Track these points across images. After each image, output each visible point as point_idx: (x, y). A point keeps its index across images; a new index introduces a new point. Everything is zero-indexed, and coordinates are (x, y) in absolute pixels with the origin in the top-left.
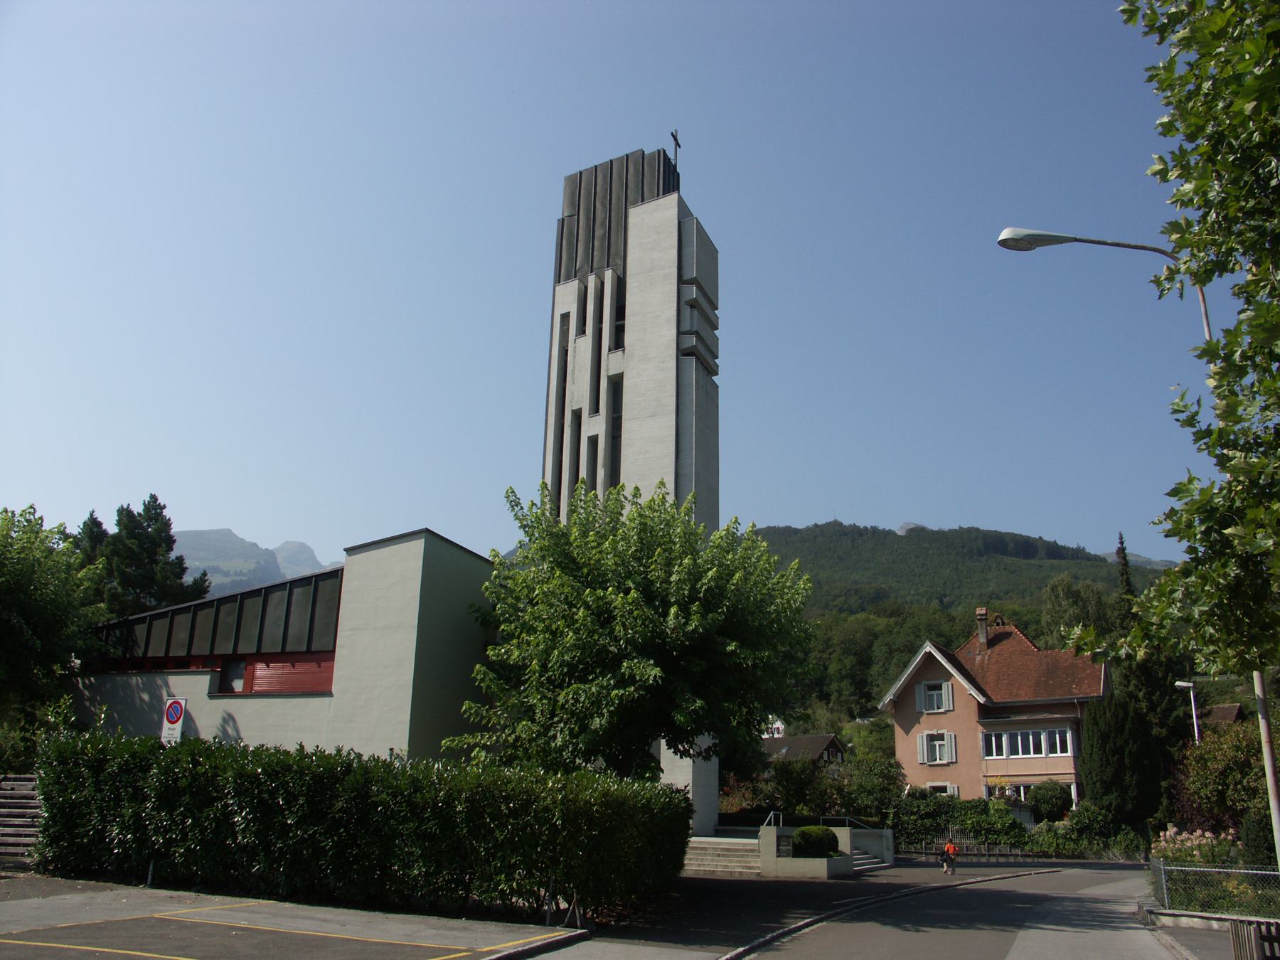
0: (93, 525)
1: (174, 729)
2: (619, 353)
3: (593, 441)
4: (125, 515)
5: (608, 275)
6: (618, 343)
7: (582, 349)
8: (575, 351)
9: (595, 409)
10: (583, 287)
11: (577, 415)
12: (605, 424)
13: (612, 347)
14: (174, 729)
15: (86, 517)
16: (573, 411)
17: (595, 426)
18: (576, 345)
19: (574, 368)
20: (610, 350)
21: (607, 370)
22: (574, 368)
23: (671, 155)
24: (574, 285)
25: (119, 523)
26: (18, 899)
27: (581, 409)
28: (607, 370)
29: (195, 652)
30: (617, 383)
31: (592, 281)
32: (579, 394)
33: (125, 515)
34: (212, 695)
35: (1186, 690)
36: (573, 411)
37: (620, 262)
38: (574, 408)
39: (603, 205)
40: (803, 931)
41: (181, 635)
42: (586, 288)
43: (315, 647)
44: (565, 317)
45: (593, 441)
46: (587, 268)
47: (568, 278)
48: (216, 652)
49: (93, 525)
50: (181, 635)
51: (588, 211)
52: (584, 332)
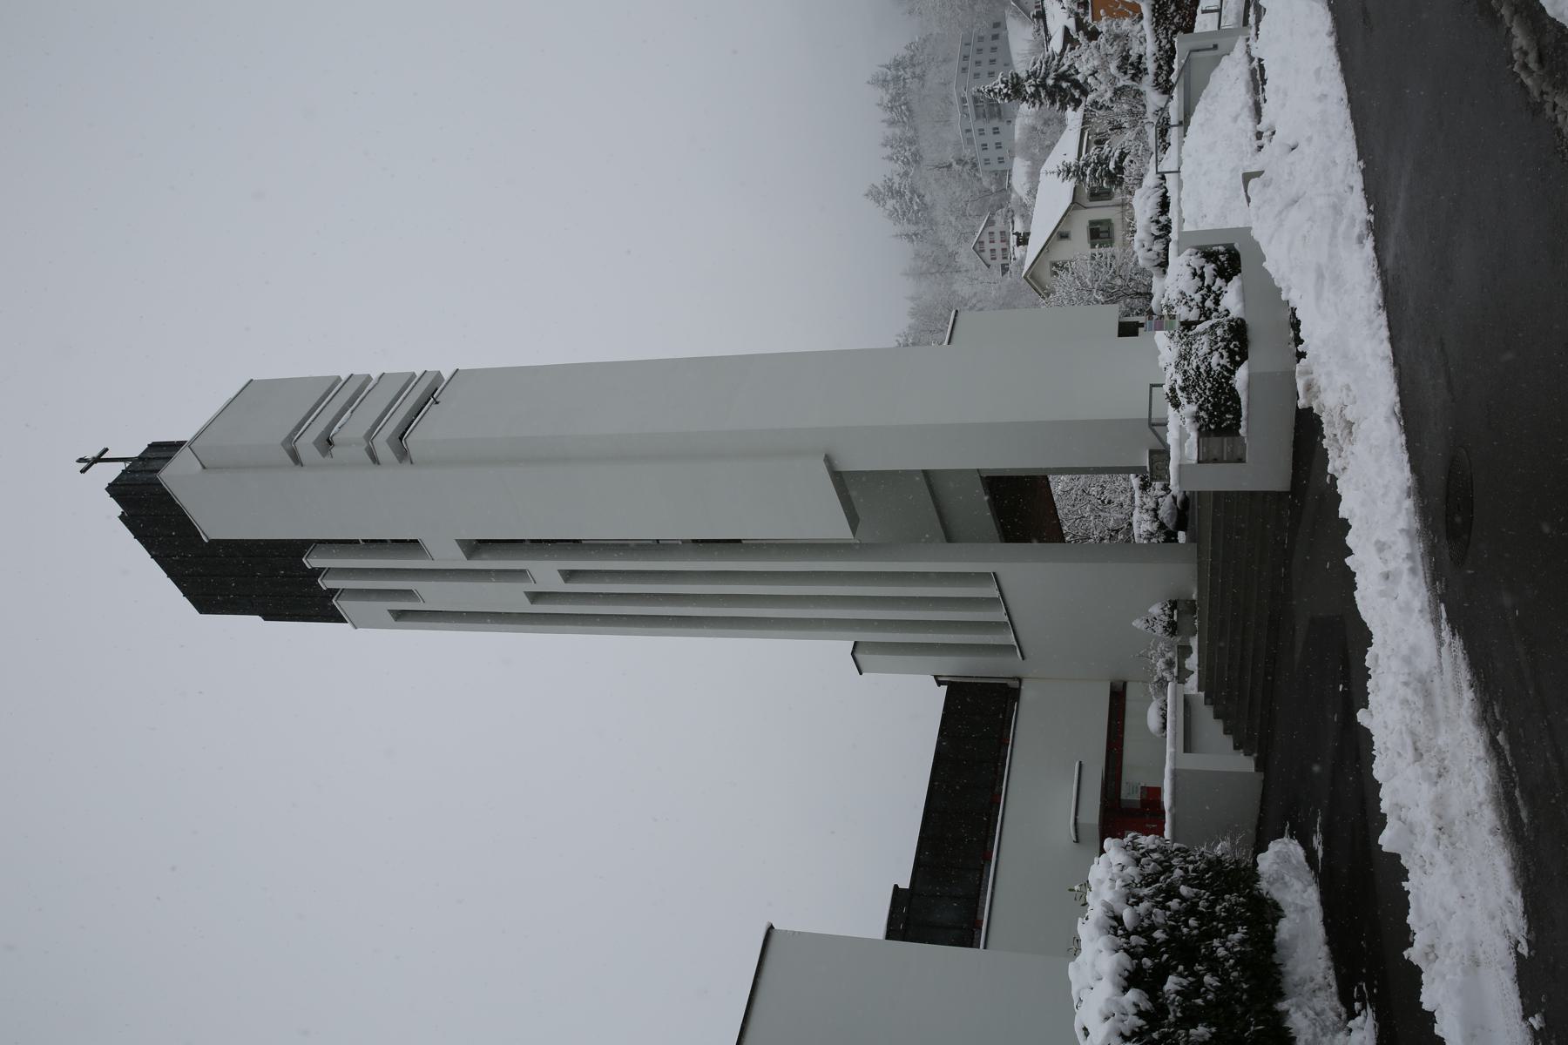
3: (569, 575)
7: (433, 594)
11: (535, 597)
17: (546, 573)
23: (114, 471)
30: (475, 547)
32: (511, 597)
44: (400, 615)
45: (569, 575)
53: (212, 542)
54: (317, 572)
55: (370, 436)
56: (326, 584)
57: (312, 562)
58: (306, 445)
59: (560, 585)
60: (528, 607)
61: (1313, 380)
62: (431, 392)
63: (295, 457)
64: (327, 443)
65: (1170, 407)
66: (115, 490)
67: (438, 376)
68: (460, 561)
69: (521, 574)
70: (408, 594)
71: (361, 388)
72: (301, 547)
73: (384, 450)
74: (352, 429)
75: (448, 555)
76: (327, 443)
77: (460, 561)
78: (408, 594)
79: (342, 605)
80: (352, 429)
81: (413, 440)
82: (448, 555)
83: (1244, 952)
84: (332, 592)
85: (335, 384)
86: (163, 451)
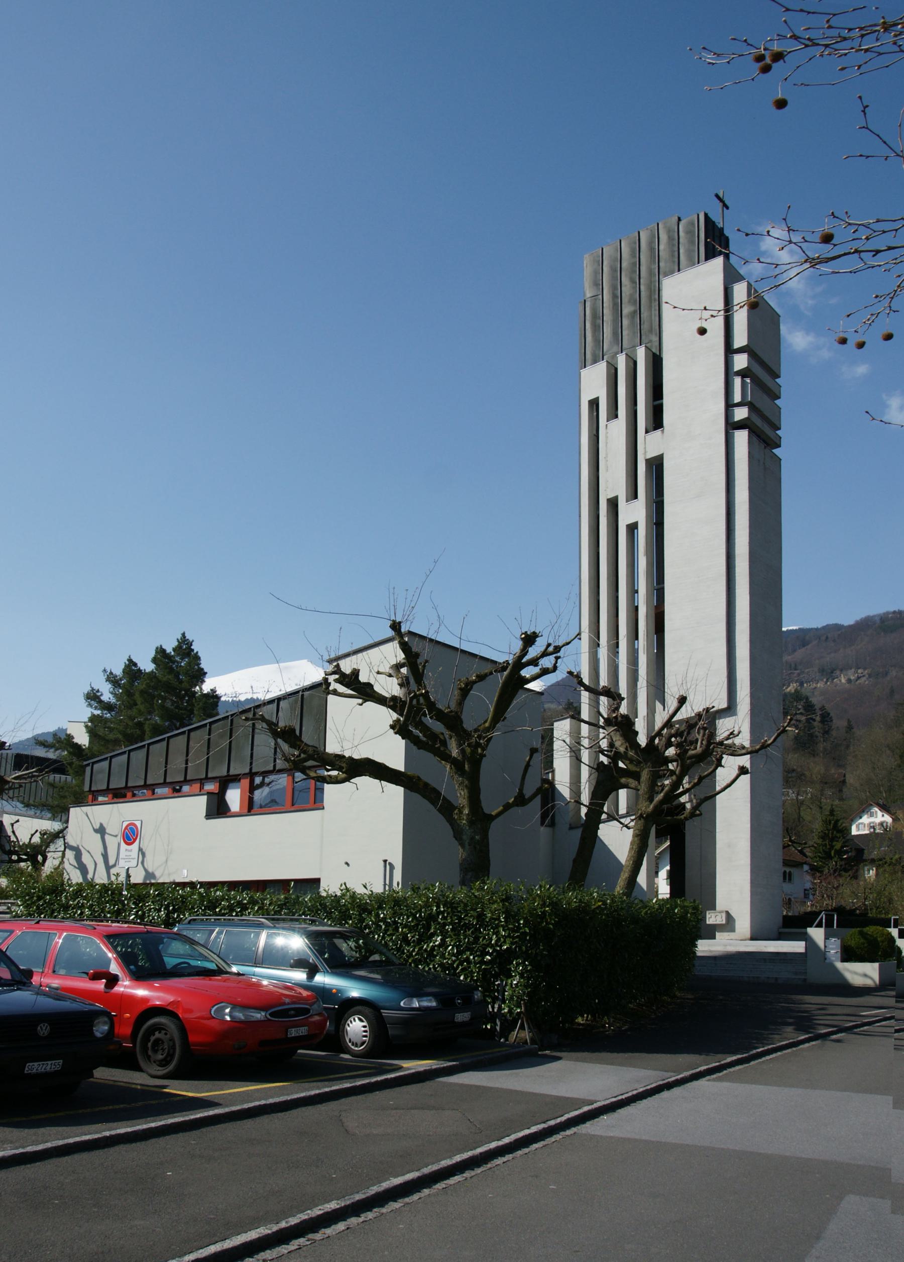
0: (131, 668)
1: (131, 850)
2: (658, 432)
4: (161, 656)
5: (641, 354)
6: (657, 421)
8: (607, 437)
9: (633, 494)
10: (632, 365)
11: (613, 504)
12: (645, 510)
13: (651, 427)
14: (131, 850)
15: (125, 660)
16: (608, 500)
18: (608, 431)
19: (607, 454)
20: (647, 432)
21: (645, 452)
22: (607, 454)
24: (601, 368)
25: (154, 660)
26: (491, 1088)
27: (616, 498)
28: (645, 452)
29: (18, 790)
30: (656, 466)
31: (622, 362)
33: (161, 656)
34: (210, 815)
35: (64, 818)
36: (608, 500)
37: (655, 339)
38: (609, 497)
39: (632, 281)
40: (801, 1046)
41: (177, 762)
42: (635, 363)
43: (148, 782)
44: (594, 404)
45: (632, 528)
46: (616, 348)
47: (595, 361)
48: (111, 787)
49: (131, 668)
50: (177, 762)
51: (613, 288)
52: (616, 417)
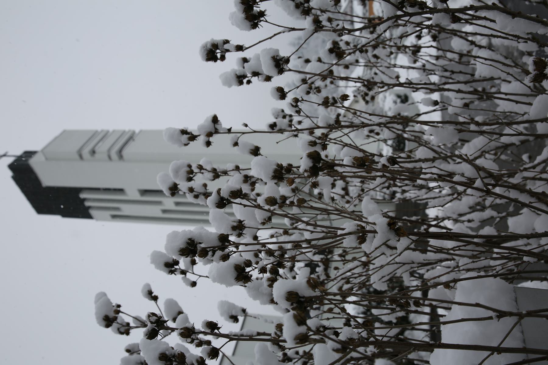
3: (177, 204)
6: (121, 191)
7: (127, 209)
11: (164, 211)
23: (10, 160)
30: (144, 192)
44: (114, 217)
53: (327, 147)
54: (84, 200)
55: (109, 150)
56: (87, 204)
57: (82, 196)
58: (86, 152)
59: (174, 207)
60: (161, 215)
61: (293, 101)
62: (132, 137)
63: (81, 157)
64: (93, 152)
65: (202, 356)
66: (11, 167)
67: (134, 133)
68: (138, 197)
69: (159, 203)
70: (118, 209)
71: (106, 135)
72: (79, 190)
73: (114, 156)
74: (102, 148)
75: (135, 195)
76: (93, 152)
77: (138, 197)
78: (118, 209)
79: (92, 212)
80: (102, 148)
81: (125, 152)
82: (135, 195)
83: (407, 307)
84: (89, 207)
85: (124, 132)
86: (29, 154)
